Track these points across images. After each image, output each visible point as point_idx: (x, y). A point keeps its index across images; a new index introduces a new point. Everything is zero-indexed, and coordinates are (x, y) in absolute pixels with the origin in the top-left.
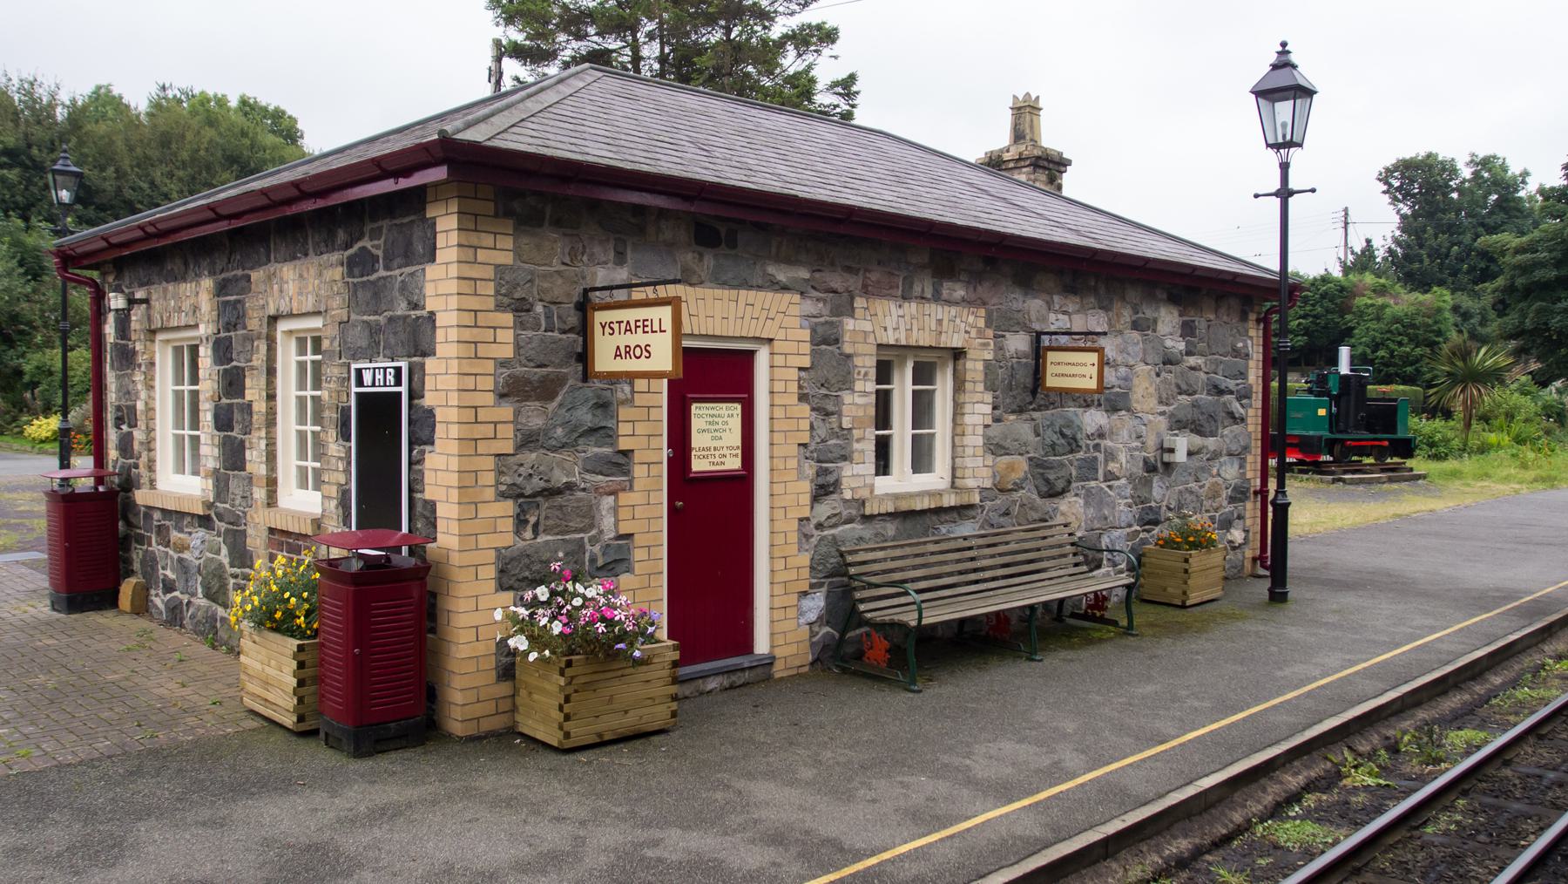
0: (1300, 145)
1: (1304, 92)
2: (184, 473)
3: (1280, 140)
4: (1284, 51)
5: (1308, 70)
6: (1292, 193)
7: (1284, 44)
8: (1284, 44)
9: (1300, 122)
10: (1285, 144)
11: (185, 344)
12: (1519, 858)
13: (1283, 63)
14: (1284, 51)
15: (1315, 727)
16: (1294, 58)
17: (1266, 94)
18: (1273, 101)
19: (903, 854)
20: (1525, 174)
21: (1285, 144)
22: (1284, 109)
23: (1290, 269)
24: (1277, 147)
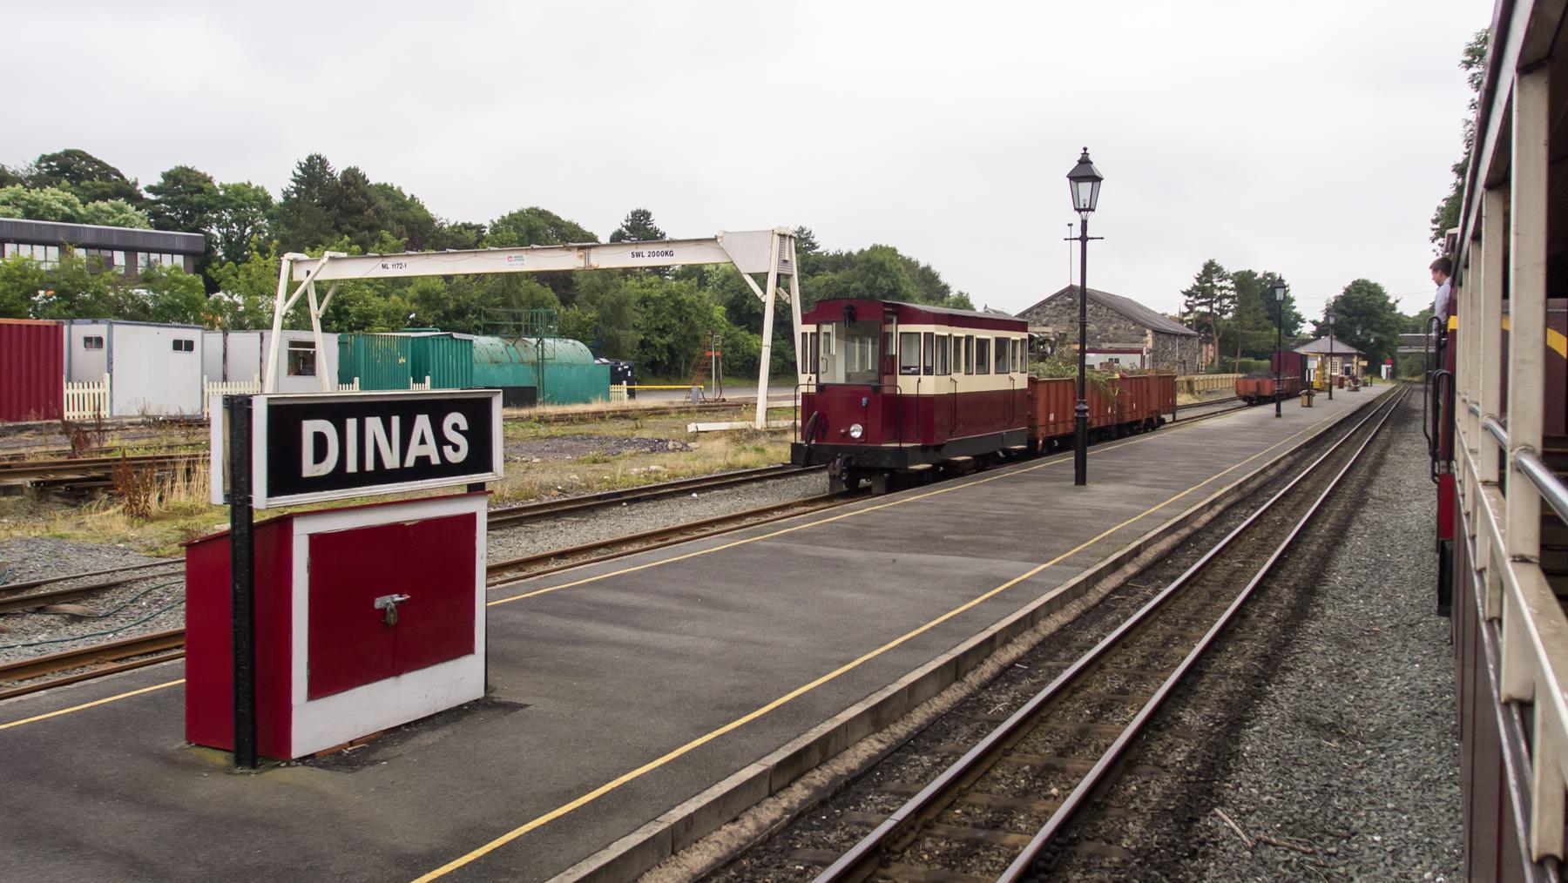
0: (1093, 210)
1: (1096, 179)
2: (989, 373)
3: (1082, 207)
4: (1085, 154)
5: (1099, 167)
6: (1080, 239)
7: (1085, 149)
8: (1085, 149)
9: (1094, 195)
10: (1085, 209)
11: (192, 324)
12: (839, 860)
13: (1085, 161)
14: (1085, 154)
15: (583, 863)
16: (1091, 158)
17: (1075, 178)
18: (1078, 182)
19: (1015, 711)
20: (1433, 229)
21: (1085, 209)
22: (1085, 188)
23: (1087, 286)
24: (1080, 210)
